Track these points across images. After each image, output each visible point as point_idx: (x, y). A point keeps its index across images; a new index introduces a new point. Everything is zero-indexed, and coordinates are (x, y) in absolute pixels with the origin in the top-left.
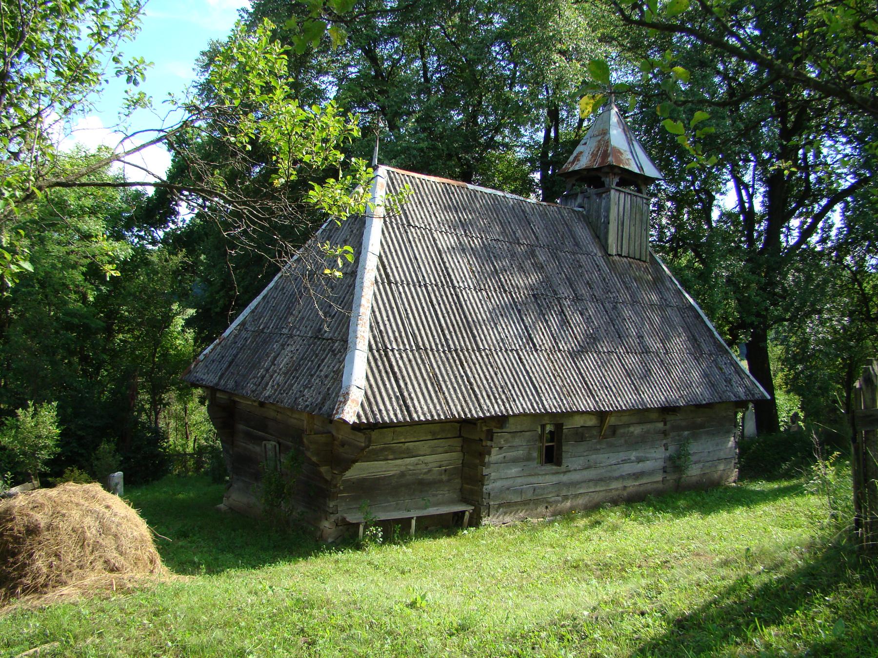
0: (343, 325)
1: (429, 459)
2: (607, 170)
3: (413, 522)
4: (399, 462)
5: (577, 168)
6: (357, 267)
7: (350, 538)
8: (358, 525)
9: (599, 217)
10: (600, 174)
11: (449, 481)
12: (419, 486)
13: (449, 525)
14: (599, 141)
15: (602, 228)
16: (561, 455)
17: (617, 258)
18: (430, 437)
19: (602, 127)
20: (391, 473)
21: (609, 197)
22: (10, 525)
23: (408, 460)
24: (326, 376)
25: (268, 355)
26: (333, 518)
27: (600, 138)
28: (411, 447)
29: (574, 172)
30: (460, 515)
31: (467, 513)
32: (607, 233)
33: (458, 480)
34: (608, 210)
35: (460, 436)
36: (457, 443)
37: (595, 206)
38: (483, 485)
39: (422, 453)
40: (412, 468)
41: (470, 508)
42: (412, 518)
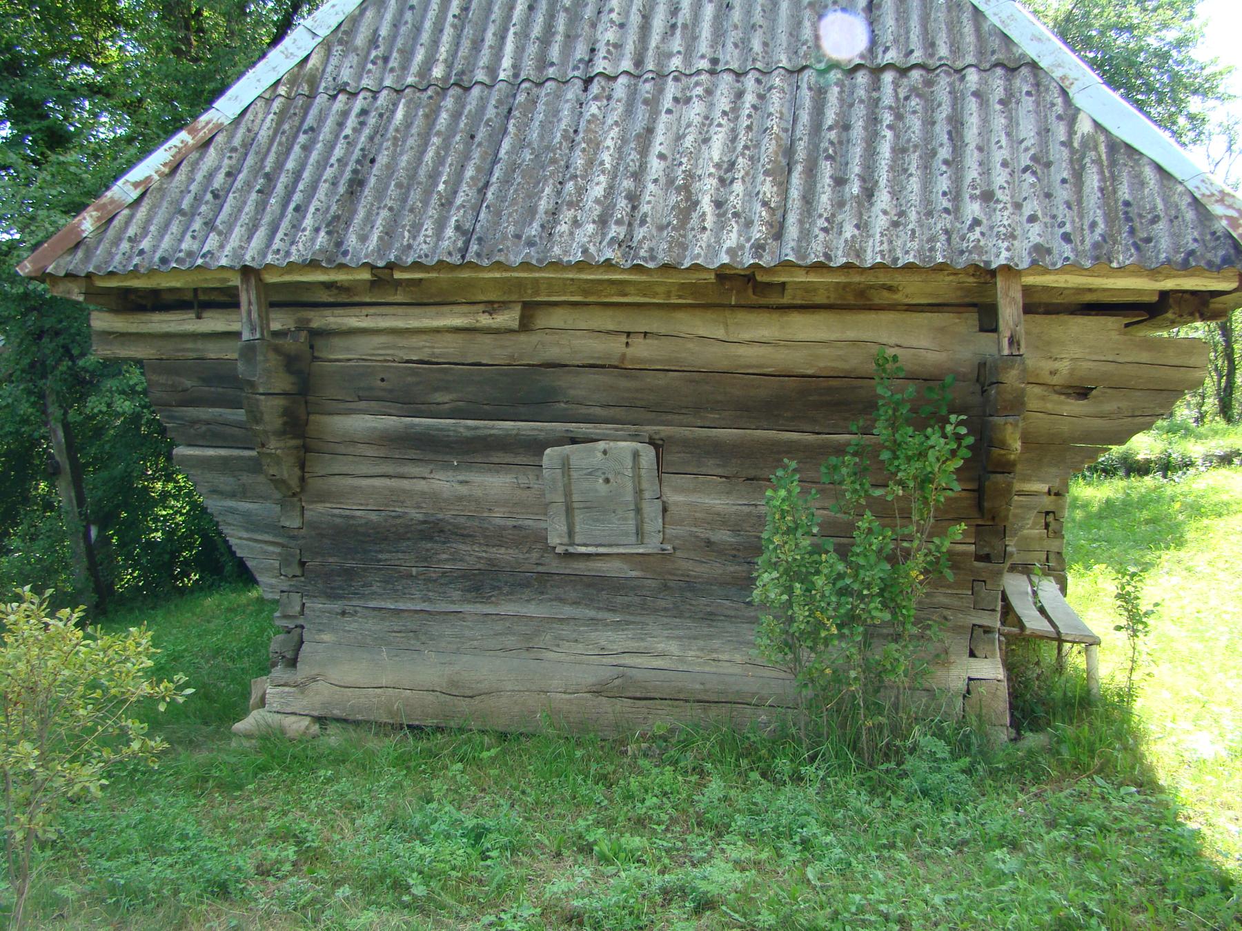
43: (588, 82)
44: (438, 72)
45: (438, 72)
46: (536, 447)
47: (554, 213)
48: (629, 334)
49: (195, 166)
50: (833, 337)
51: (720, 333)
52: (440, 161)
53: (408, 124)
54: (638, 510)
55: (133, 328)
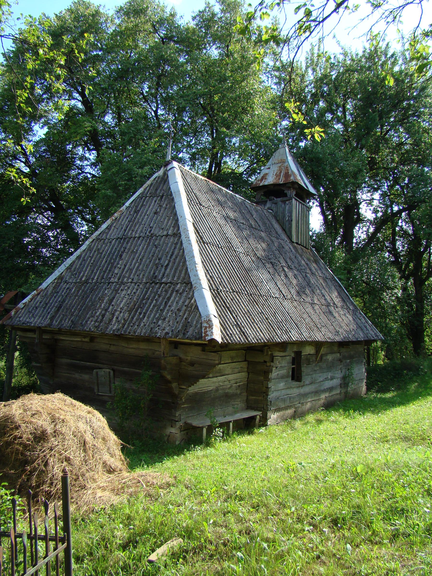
0: (181, 272)
1: (230, 377)
2: (290, 185)
3: (231, 424)
4: (215, 379)
5: (266, 183)
6: (179, 229)
7: (195, 438)
8: (202, 428)
9: (284, 216)
10: (283, 188)
11: (241, 394)
12: (226, 398)
13: (247, 426)
14: (280, 167)
15: (287, 224)
16: (301, 374)
17: (295, 244)
18: (230, 361)
19: (280, 158)
20: (211, 388)
21: (291, 204)
22: (16, 433)
23: (220, 378)
24: (179, 310)
25: (101, 299)
26: (178, 424)
27: (280, 165)
28: (221, 368)
29: (264, 186)
30: (253, 418)
31: (258, 417)
32: (291, 227)
33: (245, 394)
34: (291, 212)
35: (245, 361)
36: (244, 365)
37: (281, 209)
38: (267, 395)
39: (227, 372)
40: (221, 384)
41: (260, 413)
42: (231, 422)
43: (109, 283)
44: (83, 279)
45: (83, 279)
46: (92, 368)
47: (89, 318)
48: (111, 345)
49: (36, 299)
50: (147, 348)
51: (126, 346)
52: (75, 304)
53: (74, 292)
54: (110, 385)
55: (24, 335)
